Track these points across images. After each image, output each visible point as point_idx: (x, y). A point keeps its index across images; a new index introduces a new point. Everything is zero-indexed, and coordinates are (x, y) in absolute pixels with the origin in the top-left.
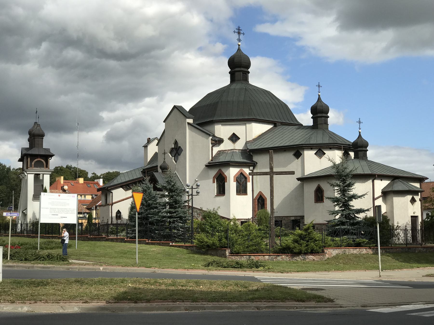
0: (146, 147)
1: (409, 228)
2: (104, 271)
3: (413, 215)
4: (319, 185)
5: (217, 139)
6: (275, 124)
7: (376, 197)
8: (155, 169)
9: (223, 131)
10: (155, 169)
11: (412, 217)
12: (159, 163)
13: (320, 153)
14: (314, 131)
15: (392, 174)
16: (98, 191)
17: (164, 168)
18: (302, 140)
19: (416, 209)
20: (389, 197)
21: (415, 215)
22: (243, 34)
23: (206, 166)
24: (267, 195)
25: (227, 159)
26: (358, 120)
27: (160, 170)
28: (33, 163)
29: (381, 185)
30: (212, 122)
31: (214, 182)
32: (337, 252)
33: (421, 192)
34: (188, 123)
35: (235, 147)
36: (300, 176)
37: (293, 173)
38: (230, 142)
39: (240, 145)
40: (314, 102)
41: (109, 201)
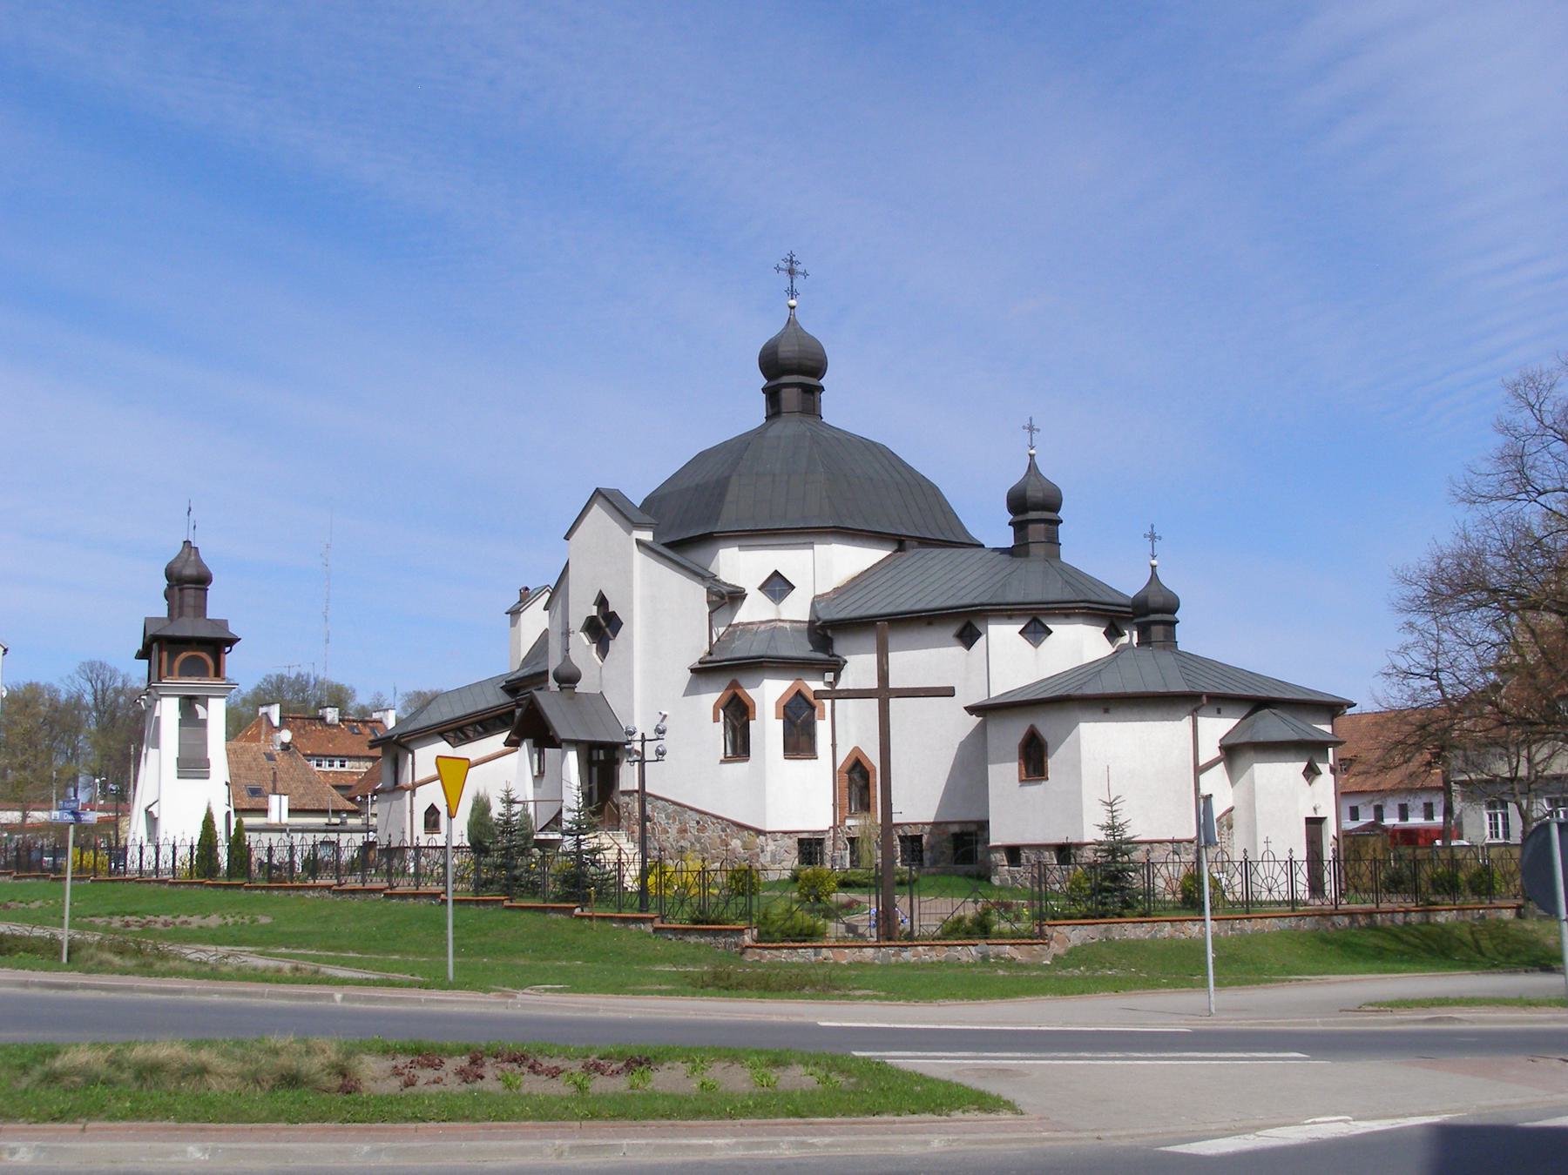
0: (515, 613)
1: (1301, 853)
2: (347, 1005)
3: (1312, 815)
4: (1032, 726)
5: (724, 590)
6: (900, 543)
7: (1202, 762)
8: (539, 678)
9: (740, 565)
10: (539, 678)
11: (1309, 821)
12: (554, 663)
13: (1036, 631)
14: (1018, 562)
15: (1250, 693)
16: (371, 748)
17: (568, 679)
18: (981, 589)
19: (1321, 796)
20: (1240, 762)
21: (1319, 815)
22: (805, 274)
23: (692, 671)
24: (874, 758)
25: (756, 650)
26: (1148, 531)
27: (553, 684)
28: (177, 664)
29: (1216, 728)
30: (709, 539)
31: (716, 720)
32: (1084, 933)
33: (1336, 744)
34: (639, 542)
35: (779, 612)
36: (978, 698)
37: (948, 692)
38: (762, 598)
39: (797, 609)
40: (1014, 475)
41: (406, 779)
